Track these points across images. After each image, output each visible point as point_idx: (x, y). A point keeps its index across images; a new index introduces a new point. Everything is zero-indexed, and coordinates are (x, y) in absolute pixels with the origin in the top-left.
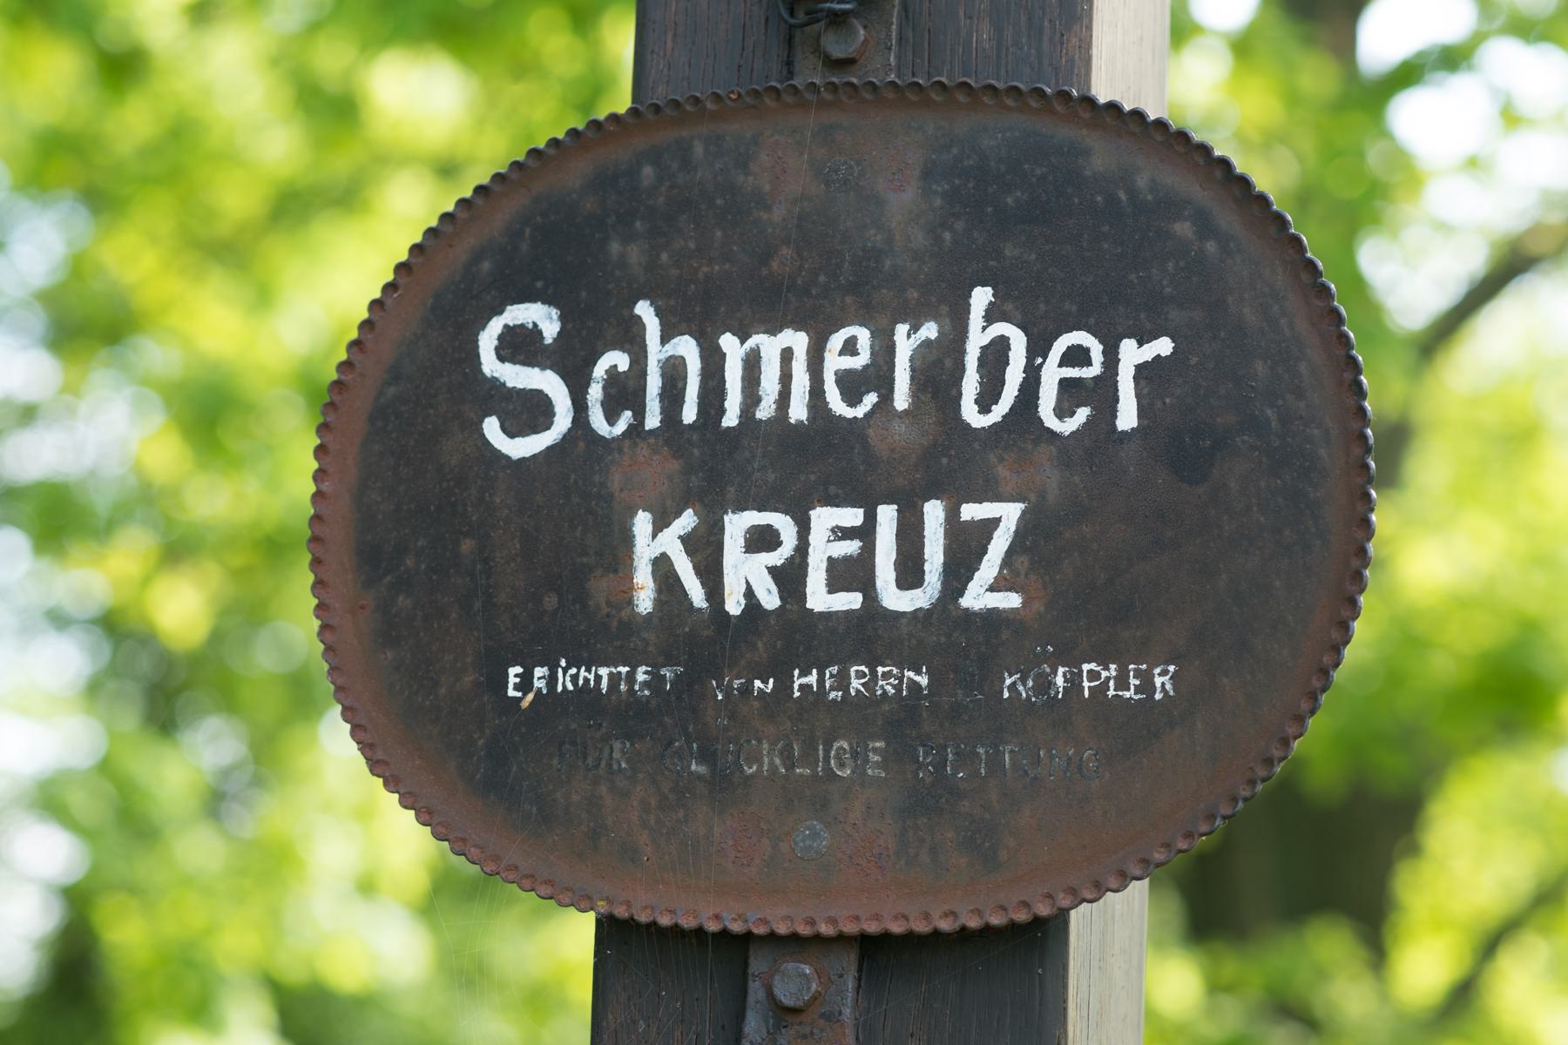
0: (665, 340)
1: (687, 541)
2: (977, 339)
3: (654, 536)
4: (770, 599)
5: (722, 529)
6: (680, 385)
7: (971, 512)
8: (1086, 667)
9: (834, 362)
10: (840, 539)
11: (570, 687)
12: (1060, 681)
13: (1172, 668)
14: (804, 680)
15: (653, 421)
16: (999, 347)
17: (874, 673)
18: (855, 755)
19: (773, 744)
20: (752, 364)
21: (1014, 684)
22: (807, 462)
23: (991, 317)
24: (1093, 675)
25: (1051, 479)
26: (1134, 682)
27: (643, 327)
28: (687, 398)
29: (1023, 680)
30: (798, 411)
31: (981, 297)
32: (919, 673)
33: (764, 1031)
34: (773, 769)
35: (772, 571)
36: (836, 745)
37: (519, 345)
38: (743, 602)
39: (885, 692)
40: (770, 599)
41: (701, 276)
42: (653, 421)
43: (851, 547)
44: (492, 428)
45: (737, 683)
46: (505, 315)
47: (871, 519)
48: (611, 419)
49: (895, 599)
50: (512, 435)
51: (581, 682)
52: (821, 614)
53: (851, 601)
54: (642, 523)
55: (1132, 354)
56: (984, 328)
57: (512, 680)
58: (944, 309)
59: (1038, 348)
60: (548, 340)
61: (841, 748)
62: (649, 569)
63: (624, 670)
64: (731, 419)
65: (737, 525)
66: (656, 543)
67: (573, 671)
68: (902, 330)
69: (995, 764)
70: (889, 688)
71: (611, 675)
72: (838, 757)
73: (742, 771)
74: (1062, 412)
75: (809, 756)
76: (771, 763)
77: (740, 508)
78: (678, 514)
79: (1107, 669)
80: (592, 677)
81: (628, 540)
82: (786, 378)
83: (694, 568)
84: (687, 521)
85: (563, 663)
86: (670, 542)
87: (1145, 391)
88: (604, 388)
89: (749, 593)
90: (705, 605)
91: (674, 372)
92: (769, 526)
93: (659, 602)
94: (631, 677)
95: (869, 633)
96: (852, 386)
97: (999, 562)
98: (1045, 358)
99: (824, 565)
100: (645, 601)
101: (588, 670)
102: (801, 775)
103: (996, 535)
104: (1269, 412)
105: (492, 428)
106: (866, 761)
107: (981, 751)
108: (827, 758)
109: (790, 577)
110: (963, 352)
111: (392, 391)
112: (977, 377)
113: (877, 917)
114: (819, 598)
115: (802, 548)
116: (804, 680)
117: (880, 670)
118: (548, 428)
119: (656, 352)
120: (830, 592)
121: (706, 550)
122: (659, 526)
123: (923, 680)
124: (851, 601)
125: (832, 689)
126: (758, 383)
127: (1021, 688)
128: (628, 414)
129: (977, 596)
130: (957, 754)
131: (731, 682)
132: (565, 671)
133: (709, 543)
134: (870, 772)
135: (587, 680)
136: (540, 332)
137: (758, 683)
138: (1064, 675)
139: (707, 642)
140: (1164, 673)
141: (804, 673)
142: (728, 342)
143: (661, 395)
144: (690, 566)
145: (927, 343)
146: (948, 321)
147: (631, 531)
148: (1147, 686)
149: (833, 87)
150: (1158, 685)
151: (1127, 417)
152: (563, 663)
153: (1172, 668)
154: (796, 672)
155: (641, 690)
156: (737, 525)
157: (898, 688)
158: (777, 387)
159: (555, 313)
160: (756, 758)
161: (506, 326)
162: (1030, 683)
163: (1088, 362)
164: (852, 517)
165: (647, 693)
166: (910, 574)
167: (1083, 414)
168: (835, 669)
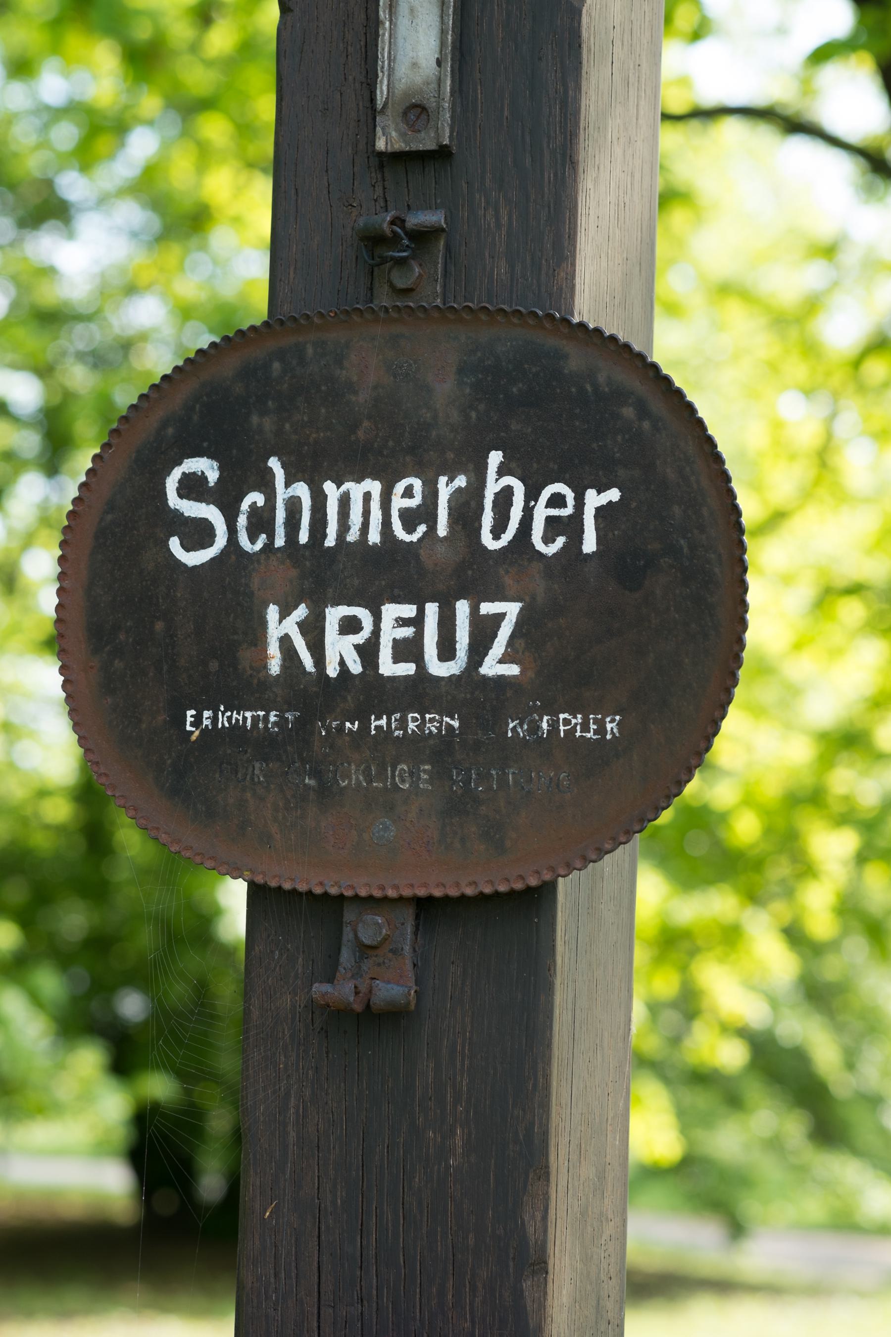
0: (287, 485)
3: (280, 622)
4: (355, 667)
6: (297, 517)
7: (486, 608)
8: (562, 716)
9: (398, 503)
10: (401, 626)
12: (545, 725)
13: (618, 718)
14: (378, 723)
15: (280, 541)
17: (423, 718)
20: (345, 502)
21: (515, 727)
22: (379, 573)
24: (567, 722)
26: (593, 727)
28: (302, 526)
29: (521, 725)
30: (374, 537)
31: (495, 458)
32: (453, 719)
34: (359, 783)
35: (357, 647)
36: (399, 767)
37: (192, 487)
38: (338, 668)
39: (431, 732)
40: (355, 667)
41: (311, 440)
42: (280, 542)
43: (408, 632)
44: (174, 544)
46: (183, 465)
47: (421, 612)
48: (253, 540)
49: (438, 668)
50: (188, 550)
51: (234, 721)
52: (389, 677)
53: (408, 669)
54: (273, 612)
55: (594, 500)
56: (497, 480)
57: (189, 719)
58: (471, 466)
59: (532, 495)
60: (212, 484)
62: (277, 644)
63: (261, 713)
64: (330, 541)
65: (334, 615)
66: (281, 626)
67: (229, 714)
68: (443, 480)
70: (433, 729)
71: (253, 717)
72: (400, 776)
73: (339, 784)
74: (548, 539)
76: (357, 779)
79: (575, 717)
80: (240, 718)
81: (264, 624)
82: (366, 513)
84: (301, 612)
85: (222, 708)
86: (291, 626)
87: (602, 526)
88: (248, 518)
89: (342, 663)
90: (313, 670)
91: (293, 506)
92: (355, 617)
93: (283, 667)
94: (266, 718)
95: (420, 691)
96: (410, 519)
97: (505, 643)
98: (536, 501)
99: (390, 644)
100: (275, 667)
101: (238, 714)
102: (376, 788)
103: (503, 624)
105: (174, 544)
106: (419, 778)
107: (494, 772)
108: (393, 777)
109: (368, 652)
111: (109, 517)
114: (388, 667)
116: (378, 723)
117: (428, 716)
118: (212, 545)
119: (282, 494)
120: (394, 663)
121: (313, 631)
122: (284, 615)
123: (456, 724)
124: (408, 669)
125: (396, 729)
127: (519, 730)
128: (264, 536)
130: (478, 774)
131: (330, 723)
134: (421, 786)
136: (206, 478)
137: (348, 724)
139: (316, 695)
140: (612, 721)
141: (378, 718)
142: (329, 487)
144: (304, 643)
145: (459, 490)
146: (473, 474)
150: (609, 729)
151: (590, 544)
152: (222, 708)
153: (618, 718)
154: (373, 717)
156: (334, 615)
157: (439, 729)
158: (361, 520)
159: (215, 464)
161: (184, 473)
162: (525, 727)
164: (409, 611)
165: (276, 729)
166: (446, 651)
167: (560, 541)
168: (398, 716)
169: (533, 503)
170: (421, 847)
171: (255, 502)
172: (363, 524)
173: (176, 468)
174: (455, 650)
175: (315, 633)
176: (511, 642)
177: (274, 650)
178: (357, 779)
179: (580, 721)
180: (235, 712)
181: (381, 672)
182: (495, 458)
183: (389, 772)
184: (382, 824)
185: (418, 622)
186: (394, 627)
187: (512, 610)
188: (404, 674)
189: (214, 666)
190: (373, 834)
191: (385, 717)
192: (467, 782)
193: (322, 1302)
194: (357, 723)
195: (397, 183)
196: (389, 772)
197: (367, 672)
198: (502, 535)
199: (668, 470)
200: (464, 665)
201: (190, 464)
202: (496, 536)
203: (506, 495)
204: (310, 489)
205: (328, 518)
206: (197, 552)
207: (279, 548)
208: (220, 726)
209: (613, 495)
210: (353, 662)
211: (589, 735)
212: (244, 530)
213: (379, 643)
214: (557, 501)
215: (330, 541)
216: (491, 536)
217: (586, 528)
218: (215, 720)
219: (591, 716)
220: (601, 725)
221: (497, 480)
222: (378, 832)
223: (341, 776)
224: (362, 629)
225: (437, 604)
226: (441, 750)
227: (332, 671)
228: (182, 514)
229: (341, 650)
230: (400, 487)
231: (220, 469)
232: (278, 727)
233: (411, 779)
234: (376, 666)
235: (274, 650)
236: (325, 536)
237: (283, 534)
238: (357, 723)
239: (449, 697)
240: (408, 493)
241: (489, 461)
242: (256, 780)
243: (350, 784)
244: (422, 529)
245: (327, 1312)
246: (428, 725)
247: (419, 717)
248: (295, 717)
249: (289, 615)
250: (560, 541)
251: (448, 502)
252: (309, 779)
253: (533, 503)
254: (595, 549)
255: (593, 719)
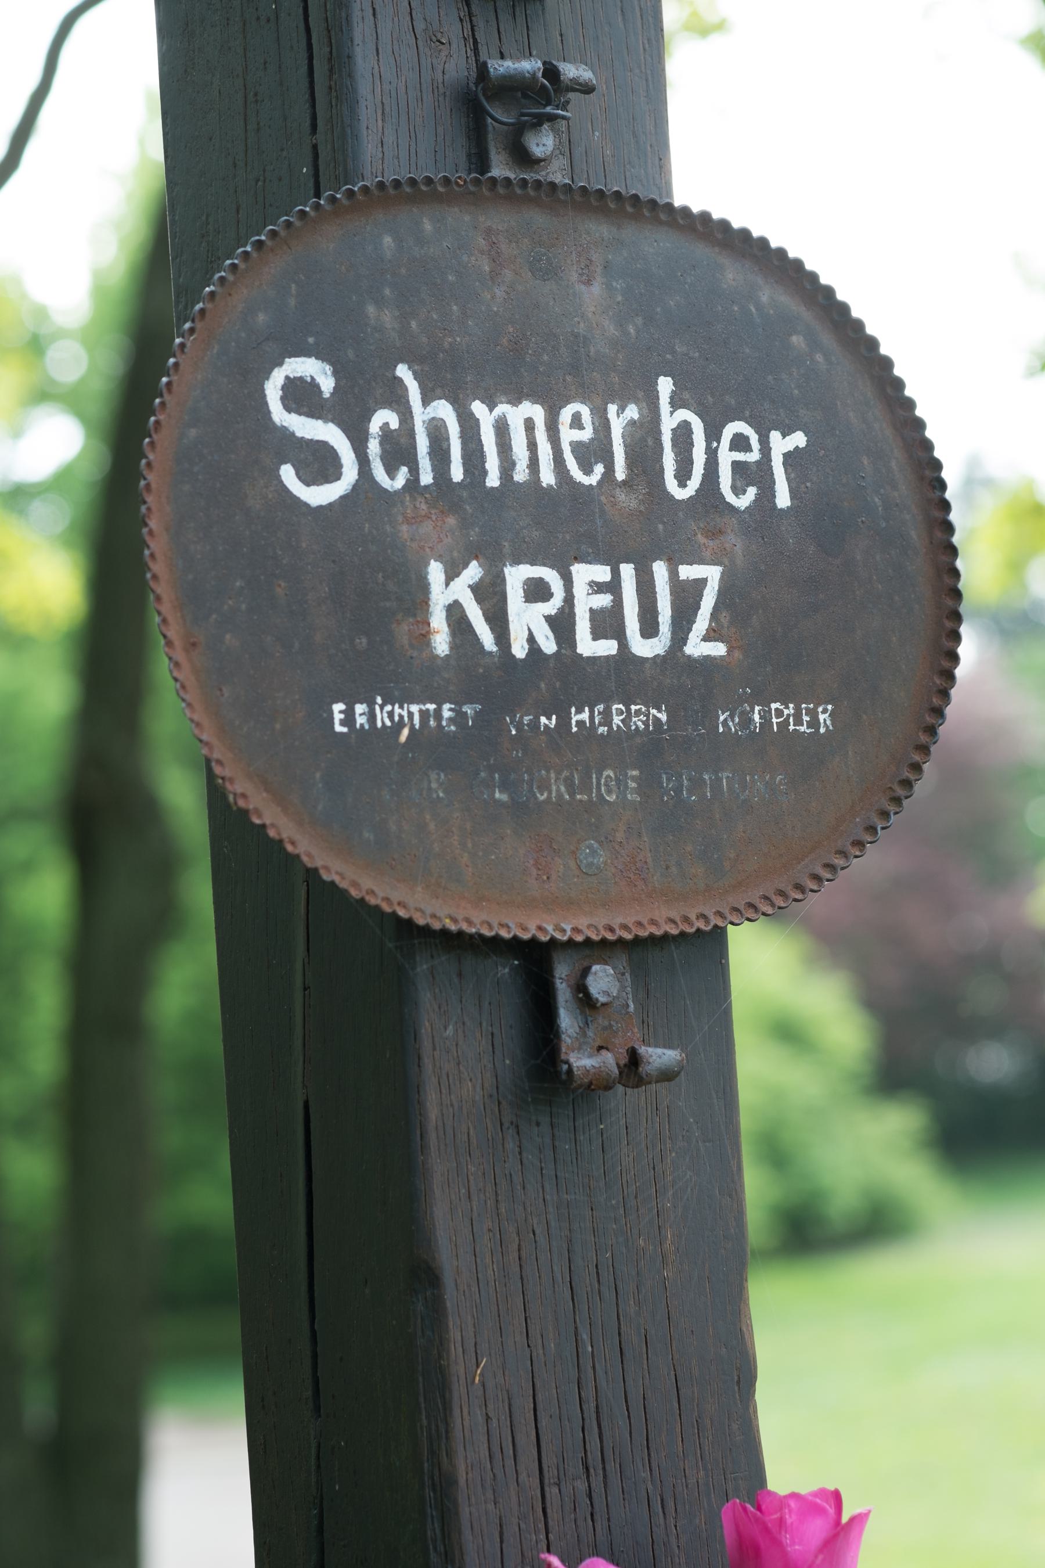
0: (426, 402)
1: (477, 590)
2: (669, 422)
3: (447, 585)
4: (549, 645)
5: (504, 580)
6: (445, 446)
7: (688, 572)
8: (774, 706)
9: (568, 436)
10: (597, 592)
11: (388, 723)
12: (756, 717)
13: (830, 707)
14: (580, 717)
15: (426, 478)
16: (683, 432)
17: (629, 710)
18: (618, 781)
19: (558, 773)
20: (502, 429)
21: (725, 720)
22: (558, 524)
23: (676, 403)
24: (779, 713)
25: (735, 542)
26: (806, 718)
27: (406, 389)
28: (453, 458)
29: (732, 716)
30: (548, 477)
31: (665, 386)
32: (660, 711)
33: (576, 1024)
34: (559, 795)
35: (548, 619)
36: (605, 773)
37: (301, 396)
38: (527, 647)
39: (637, 727)
40: (549, 645)
41: (446, 345)
42: (426, 478)
43: (604, 600)
44: (288, 474)
45: (526, 719)
46: (285, 367)
47: (616, 573)
48: (391, 472)
49: (644, 648)
50: (308, 484)
51: (396, 718)
52: (589, 658)
53: (608, 647)
54: (435, 572)
55: (781, 444)
56: (672, 413)
57: (338, 717)
58: (640, 394)
59: (713, 434)
60: (327, 395)
61: (608, 776)
62: (444, 614)
63: (431, 707)
64: (493, 480)
65: (516, 576)
66: (450, 589)
67: (389, 708)
68: (612, 409)
69: (716, 784)
70: (640, 724)
71: (420, 711)
72: (606, 785)
73: (536, 798)
74: (738, 491)
75: (586, 787)
76: (558, 790)
77: (517, 561)
78: (466, 565)
79: (787, 708)
80: (405, 713)
81: (425, 588)
82: (532, 446)
83: (484, 615)
84: (473, 572)
85: (379, 700)
86: (461, 590)
87: (793, 475)
88: (381, 444)
89: (531, 639)
90: (495, 649)
91: (437, 433)
92: (541, 579)
93: (453, 646)
94: (438, 713)
95: (623, 676)
96: (586, 455)
97: (709, 616)
98: (719, 443)
99: (587, 615)
100: (441, 643)
101: (401, 707)
102: (581, 801)
103: (705, 592)
104: (877, 500)
105: (288, 474)
106: (626, 787)
107: (706, 777)
108: (599, 784)
109: (562, 624)
110: (659, 433)
111: (193, 432)
112: (673, 455)
113: (653, 922)
114: (587, 646)
115: (569, 599)
116: (580, 717)
117: (633, 708)
118: (339, 479)
119: (420, 415)
120: (594, 639)
121: (491, 596)
122: (451, 576)
123: (663, 717)
124: (608, 647)
125: (600, 724)
126: (510, 448)
127: (731, 724)
128: (404, 470)
129: (697, 647)
130: (689, 780)
131: (521, 717)
132: (382, 707)
133: (495, 593)
134: (629, 796)
135: (401, 717)
136: (318, 387)
137: (543, 720)
138: (759, 713)
139: (499, 683)
140: (825, 711)
141: (579, 711)
142: (478, 408)
143: (429, 454)
144: (480, 613)
145: (632, 423)
146: (644, 404)
147: (426, 578)
148: (814, 723)
149: (524, 183)
150: (822, 721)
151: (783, 499)
152: (379, 700)
153: (830, 707)
154: (573, 710)
155: (448, 725)
156: (516, 576)
157: (646, 723)
158: (527, 454)
159: (328, 368)
160: (544, 786)
161: (287, 378)
162: (737, 720)
163: (748, 448)
164: (602, 573)
165: (453, 728)
166: (649, 628)
167: (752, 492)
168: (601, 707)
169: (715, 444)
170: (635, 874)
171: (387, 424)
172: (530, 459)
173: (276, 370)
174: (658, 623)
175: (495, 600)
176: (714, 615)
177: (438, 621)
178: (558, 790)
179: (792, 711)
180: (397, 706)
181: (579, 651)
182: (665, 386)
183: (594, 780)
184: (588, 847)
185: (613, 587)
186: (589, 594)
187: (712, 574)
188: (606, 654)
189: (362, 642)
190: (581, 861)
191: (587, 709)
192: (678, 790)
193: (546, 1481)
194: (554, 717)
195: (487, 21)
196: (594, 780)
197: (563, 651)
198: (688, 482)
199: (851, 414)
200: (668, 644)
201: (294, 366)
202: (682, 484)
203: (683, 432)
204: (456, 410)
205: (485, 449)
206: (322, 488)
207: (426, 487)
208: (379, 724)
209: (799, 439)
210: (544, 639)
211: (803, 729)
212: (378, 460)
213: (575, 614)
214: (740, 443)
215: (493, 480)
216: (676, 482)
217: (776, 477)
218: (372, 717)
219: (804, 706)
220: (813, 714)
221: (672, 413)
222: (586, 858)
223: (539, 787)
224: (551, 595)
225: (632, 566)
226: (649, 750)
227: (519, 650)
228: (293, 434)
229: (528, 623)
230: (566, 415)
231: (335, 373)
232: (455, 725)
233: (616, 787)
234: (573, 645)
235: (438, 621)
236: (485, 473)
237: (429, 468)
238: (554, 717)
239: (655, 683)
240: (577, 422)
241: (659, 388)
242: (435, 796)
243: (549, 797)
244: (599, 469)
245: (552, 1492)
246: (634, 719)
247: (623, 708)
248: (476, 711)
249: (458, 575)
250: (752, 492)
251: (623, 437)
252: (500, 792)
253: (715, 444)
254: (789, 504)
255: (806, 709)
